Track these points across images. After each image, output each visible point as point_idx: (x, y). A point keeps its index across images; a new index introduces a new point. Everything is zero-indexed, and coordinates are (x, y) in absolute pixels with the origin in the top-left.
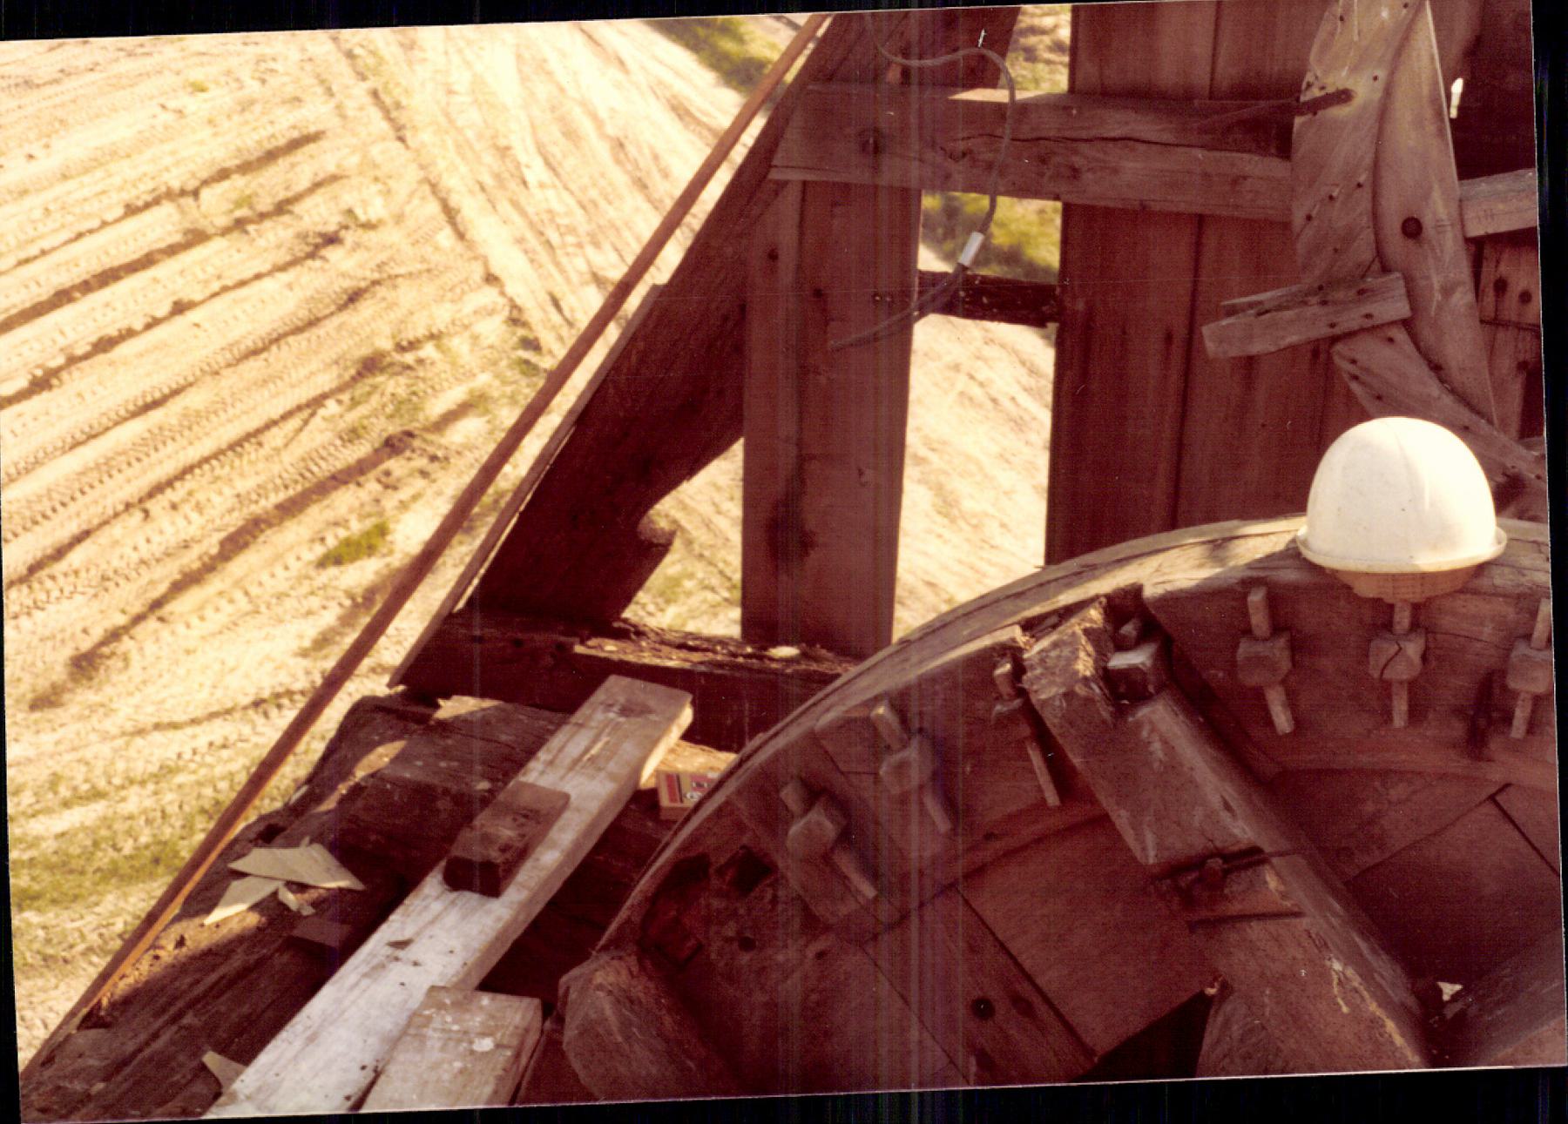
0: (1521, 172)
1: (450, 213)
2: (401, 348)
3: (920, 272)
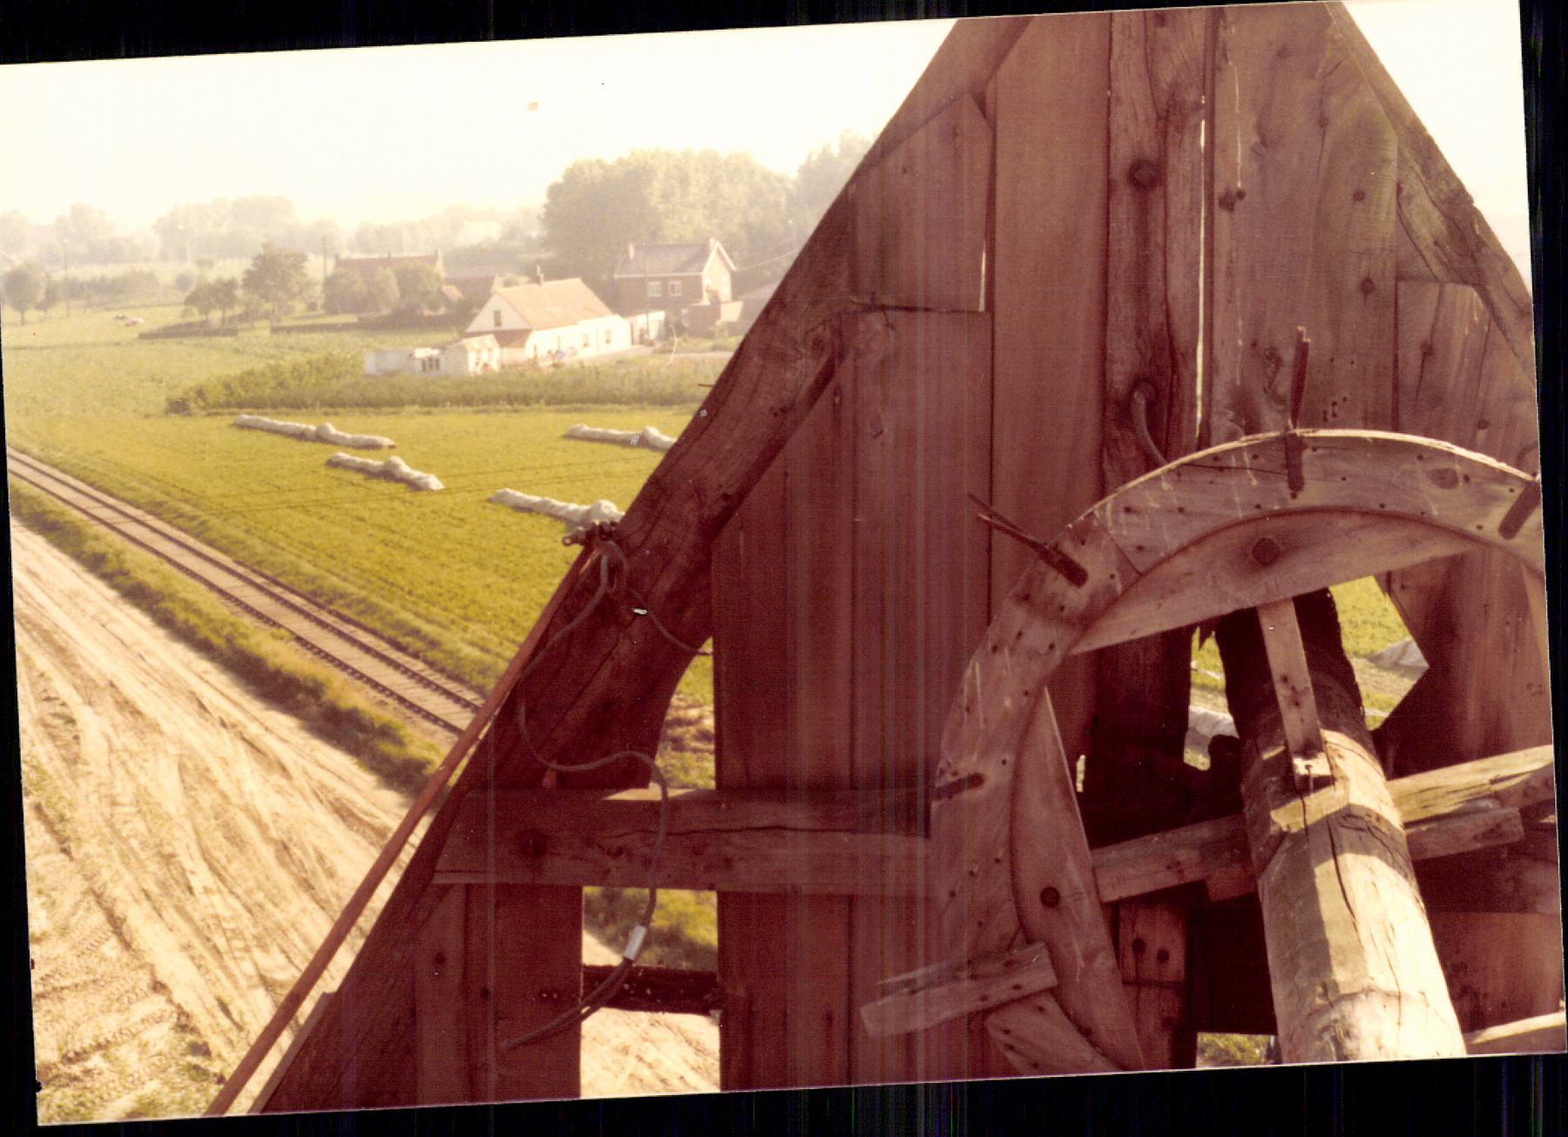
0: (1147, 837)
1: (116, 923)
2: (67, 1060)
3: (585, 967)
